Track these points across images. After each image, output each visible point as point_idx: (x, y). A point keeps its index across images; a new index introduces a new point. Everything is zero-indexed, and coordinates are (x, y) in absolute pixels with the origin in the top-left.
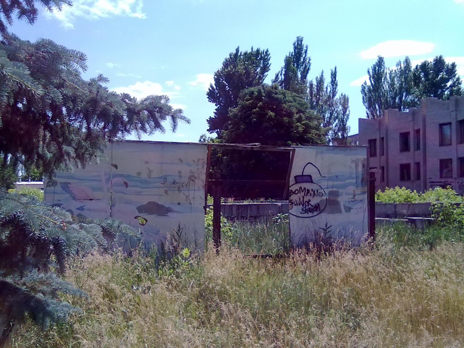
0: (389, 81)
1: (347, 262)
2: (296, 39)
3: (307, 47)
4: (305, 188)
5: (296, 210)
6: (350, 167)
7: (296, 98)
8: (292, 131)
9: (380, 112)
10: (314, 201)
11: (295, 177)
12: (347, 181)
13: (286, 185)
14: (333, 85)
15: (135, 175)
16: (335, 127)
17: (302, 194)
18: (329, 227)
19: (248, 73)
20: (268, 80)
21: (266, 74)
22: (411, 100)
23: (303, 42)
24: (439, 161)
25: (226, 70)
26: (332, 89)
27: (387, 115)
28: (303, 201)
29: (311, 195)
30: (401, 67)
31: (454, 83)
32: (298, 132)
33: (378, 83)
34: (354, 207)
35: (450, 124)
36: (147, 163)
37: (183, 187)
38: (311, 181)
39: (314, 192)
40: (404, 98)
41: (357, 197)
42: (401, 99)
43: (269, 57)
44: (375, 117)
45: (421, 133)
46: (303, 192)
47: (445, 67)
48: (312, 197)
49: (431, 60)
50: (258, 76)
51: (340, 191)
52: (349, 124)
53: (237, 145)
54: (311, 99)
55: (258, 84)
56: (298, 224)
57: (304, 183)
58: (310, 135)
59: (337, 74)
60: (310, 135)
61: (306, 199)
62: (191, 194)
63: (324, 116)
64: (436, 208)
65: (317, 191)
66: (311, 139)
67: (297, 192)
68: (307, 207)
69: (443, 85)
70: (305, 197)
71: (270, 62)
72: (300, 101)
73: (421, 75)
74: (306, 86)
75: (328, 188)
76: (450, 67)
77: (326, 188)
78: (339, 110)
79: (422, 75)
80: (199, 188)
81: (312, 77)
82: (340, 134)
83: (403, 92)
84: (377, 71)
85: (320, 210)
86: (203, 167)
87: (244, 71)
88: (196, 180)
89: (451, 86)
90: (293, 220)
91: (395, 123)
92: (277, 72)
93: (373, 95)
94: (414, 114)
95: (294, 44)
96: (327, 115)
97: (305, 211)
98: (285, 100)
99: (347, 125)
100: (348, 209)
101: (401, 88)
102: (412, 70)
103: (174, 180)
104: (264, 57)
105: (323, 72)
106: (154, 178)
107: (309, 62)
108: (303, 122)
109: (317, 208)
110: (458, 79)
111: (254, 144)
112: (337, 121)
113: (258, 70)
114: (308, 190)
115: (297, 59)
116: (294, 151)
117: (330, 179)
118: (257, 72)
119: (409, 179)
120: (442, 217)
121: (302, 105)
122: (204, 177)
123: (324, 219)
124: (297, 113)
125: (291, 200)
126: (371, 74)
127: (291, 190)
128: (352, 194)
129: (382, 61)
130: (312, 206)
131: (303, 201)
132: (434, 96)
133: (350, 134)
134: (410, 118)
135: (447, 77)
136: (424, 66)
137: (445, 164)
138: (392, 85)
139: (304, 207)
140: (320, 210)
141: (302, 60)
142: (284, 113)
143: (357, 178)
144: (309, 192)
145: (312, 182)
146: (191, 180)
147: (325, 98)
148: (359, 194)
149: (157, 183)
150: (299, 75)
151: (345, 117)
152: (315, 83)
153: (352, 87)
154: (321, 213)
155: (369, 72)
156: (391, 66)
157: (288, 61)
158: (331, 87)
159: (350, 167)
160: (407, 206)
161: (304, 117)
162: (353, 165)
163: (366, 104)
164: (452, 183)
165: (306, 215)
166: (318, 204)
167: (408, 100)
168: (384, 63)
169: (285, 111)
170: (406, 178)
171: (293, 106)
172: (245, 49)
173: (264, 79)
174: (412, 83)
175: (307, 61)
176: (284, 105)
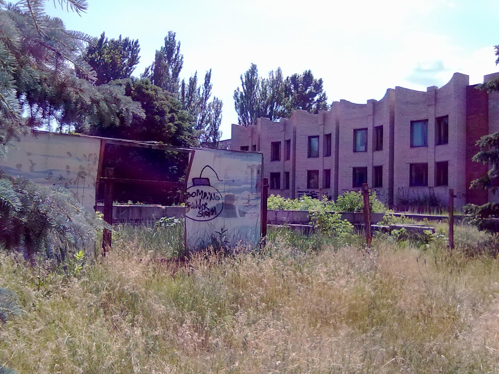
0: (261, 90)
1: (247, 265)
2: (167, 34)
3: (179, 43)
4: (202, 191)
5: (192, 213)
6: (246, 173)
7: (169, 96)
8: (164, 132)
9: (251, 120)
10: (211, 205)
11: (193, 179)
12: (243, 186)
13: (184, 186)
14: (206, 88)
15: (15, 168)
16: (207, 130)
17: (199, 197)
18: (224, 231)
19: (114, 64)
20: (137, 73)
21: (134, 66)
22: (281, 110)
23: (175, 38)
24: (307, 172)
25: (90, 56)
26: (205, 91)
27: (259, 124)
28: (200, 204)
29: (207, 198)
30: (273, 77)
31: (321, 98)
32: (170, 133)
33: (251, 90)
34: (249, 212)
35: (318, 137)
36: (29, 154)
37: (71, 184)
38: (208, 184)
39: (211, 195)
40: (274, 108)
41: (251, 202)
42: (271, 108)
43: (138, 49)
44: (247, 124)
45: (292, 143)
46: (200, 194)
47: (314, 82)
48: (209, 200)
49: (300, 73)
50: (125, 68)
51: (236, 195)
52: (221, 129)
53: (135, 141)
54: (183, 99)
55: (125, 76)
56: (195, 227)
57: (202, 186)
58: (183, 137)
59: (211, 76)
60: (183, 137)
61: (203, 202)
62: (80, 191)
63: (196, 118)
64: (314, 216)
65: (214, 195)
66: (183, 140)
67: (194, 194)
68: (204, 210)
69: (310, 99)
70: (202, 200)
71: (139, 55)
72: (173, 100)
73: (291, 87)
74: (178, 85)
75: (224, 192)
76: (317, 82)
77: (222, 192)
78: (211, 113)
79: (292, 87)
80: (89, 186)
81: (184, 76)
82: (211, 138)
83: (274, 102)
84: (250, 78)
85: (216, 214)
86: (95, 162)
87: (111, 61)
88: (87, 177)
89: (317, 100)
90: (190, 224)
91: (267, 132)
92: (147, 67)
93: (246, 102)
94: (285, 124)
95: (166, 39)
96: (199, 117)
97: (202, 214)
98: (157, 97)
99: (219, 130)
100: (243, 214)
101: (273, 97)
102: (283, 81)
103: (60, 175)
104: (133, 49)
105: (196, 73)
106: (38, 172)
107: (181, 60)
108: (176, 123)
109: (213, 211)
110: (324, 95)
111: (153, 142)
112: (209, 125)
113: (126, 61)
114: (205, 194)
115: (169, 53)
116: (193, 152)
117: (226, 183)
118: (125, 63)
119: (278, 187)
120: (319, 225)
121: (175, 105)
122: (95, 174)
123: (219, 222)
124: (169, 113)
125: (188, 203)
126: (244, 80)
127: (189, 193)
128: (246, 199)
129: (255, 68)
130: (208, 209)
131: (200, 204)
132: (302, 109)
133: (221, 139)
134: (282, 128)
135: (314, 91)
136: (294, 79)
137: (311, 174)
138: (264, 94)
139: (201, 210)
140: (216, 214)
141: (174, 56)
142: (155, 110)
143: (252, 183)
144: (206, 195)
145: (209, 185)
146: (80, 177)
147: (198, 100)
148: (252, 199)
149: (41, 177)
150: (171, 72)
151: (217, 121)
152: (187, 83)
153: (225, 91)
154: (216, 217)
155: (241, 78)
156: (263, 75)
157: (159, 57)
158: (204, 89)
159: (246, 173)
160: (287, 213)
161: (176, 117)
162: (249, 171)
163: (238, 110)
164: (317, 194)
165: (202, 218)
166: (215, 208)
167: (279, 111)
168: (257, 71)
169: (157, 109)
170: (275, 187)
171: (165, 104)
172: (112, 35)
173: (132, 72)
174: (283, 94)
175: (180, 58)
176: (156, 102)
